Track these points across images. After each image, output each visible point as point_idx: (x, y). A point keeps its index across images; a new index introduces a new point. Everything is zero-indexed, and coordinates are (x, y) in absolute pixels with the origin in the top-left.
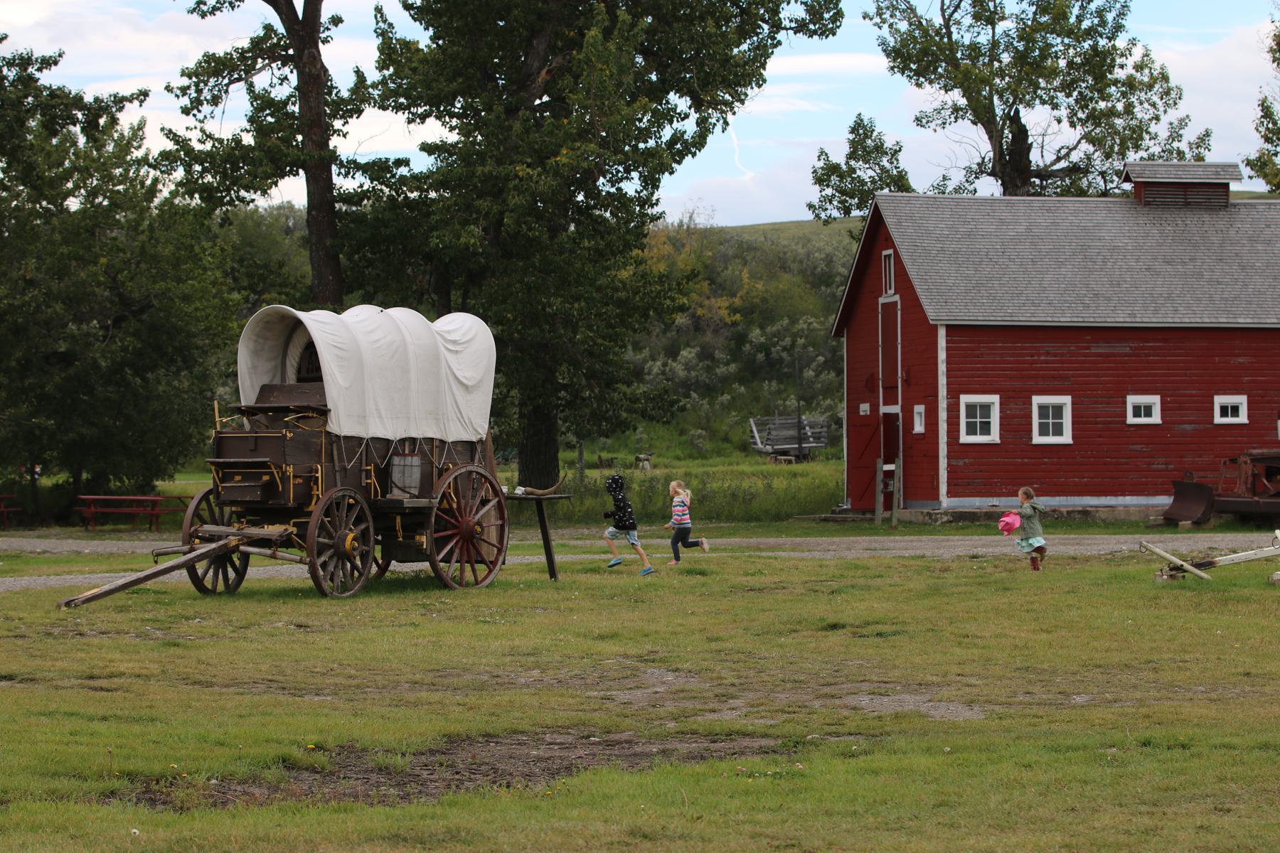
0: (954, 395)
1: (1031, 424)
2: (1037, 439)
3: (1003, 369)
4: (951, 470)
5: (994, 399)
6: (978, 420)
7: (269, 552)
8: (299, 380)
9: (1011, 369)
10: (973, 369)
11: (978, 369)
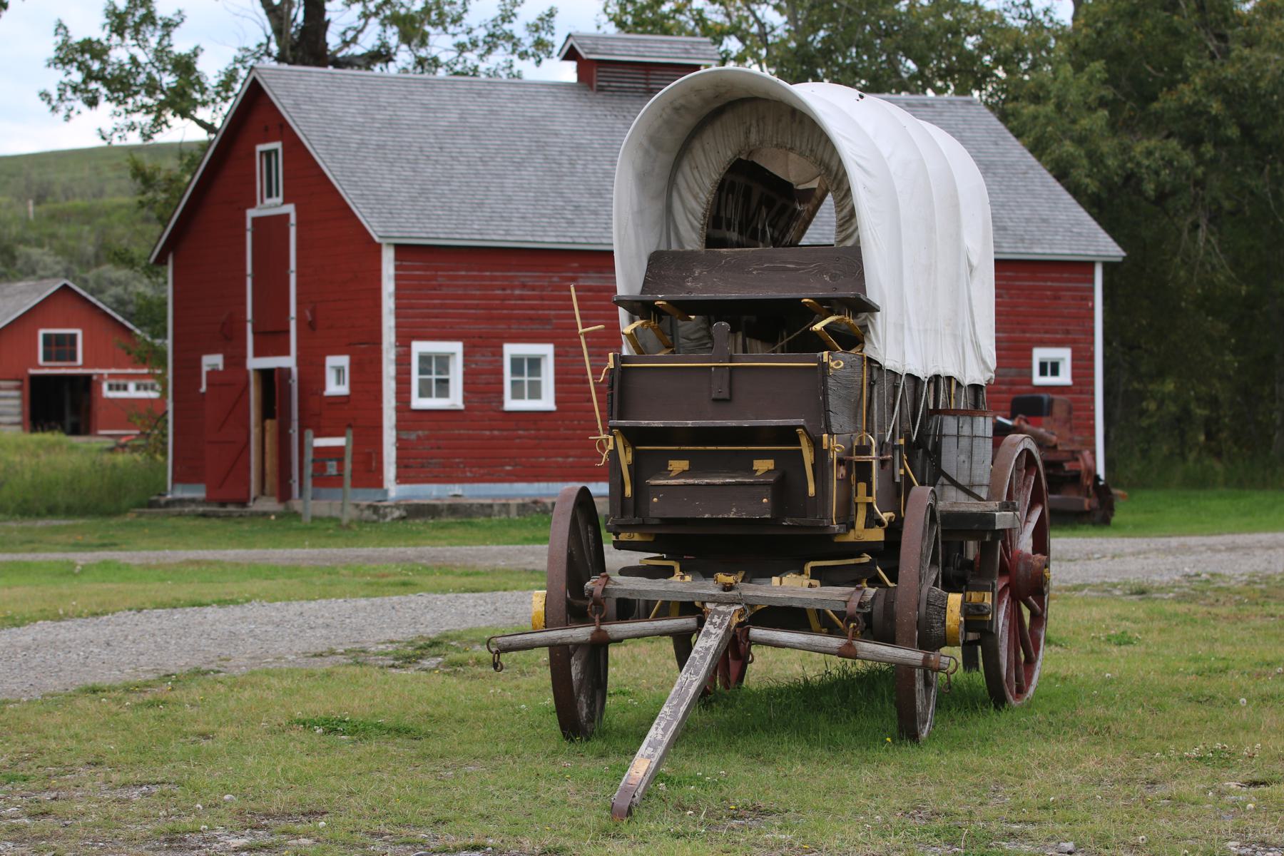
0: (404, 342)
1: (501, 382)
2: (510, 404)
3: (466, 307)
4: (401, 446)
5: (456, 348)
6: (433, 374)
7: (835, 642)
8: (711, 242)
9: (476, 307)
10: (428, 306)
11: (435, 307)
